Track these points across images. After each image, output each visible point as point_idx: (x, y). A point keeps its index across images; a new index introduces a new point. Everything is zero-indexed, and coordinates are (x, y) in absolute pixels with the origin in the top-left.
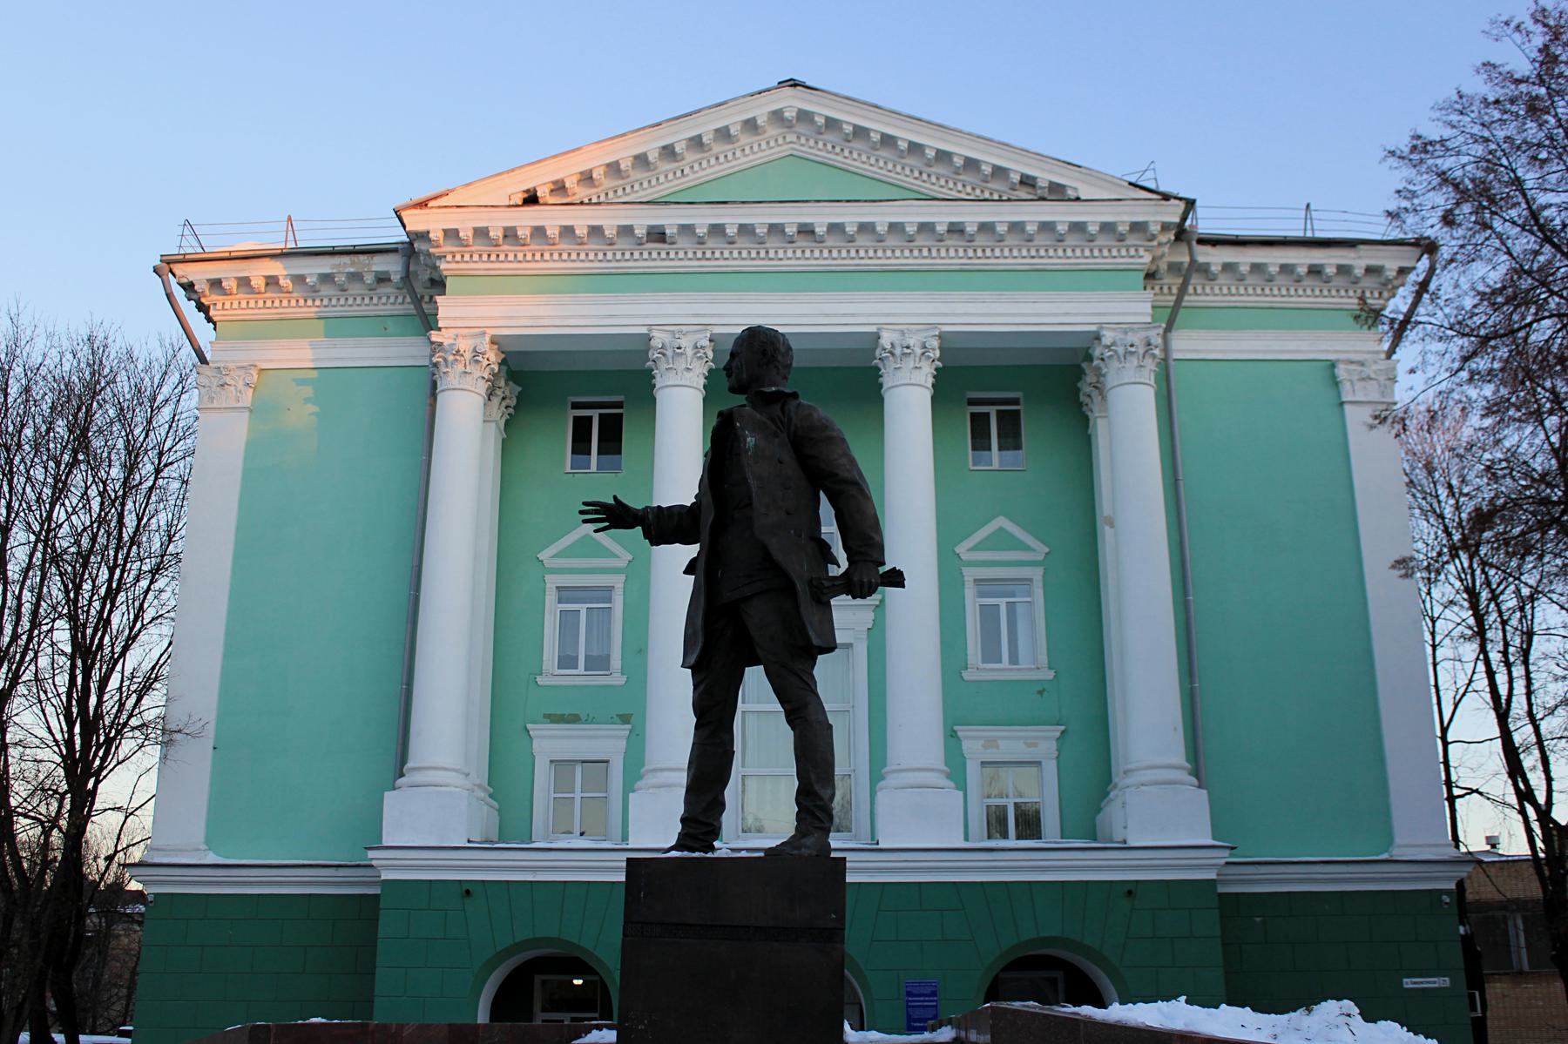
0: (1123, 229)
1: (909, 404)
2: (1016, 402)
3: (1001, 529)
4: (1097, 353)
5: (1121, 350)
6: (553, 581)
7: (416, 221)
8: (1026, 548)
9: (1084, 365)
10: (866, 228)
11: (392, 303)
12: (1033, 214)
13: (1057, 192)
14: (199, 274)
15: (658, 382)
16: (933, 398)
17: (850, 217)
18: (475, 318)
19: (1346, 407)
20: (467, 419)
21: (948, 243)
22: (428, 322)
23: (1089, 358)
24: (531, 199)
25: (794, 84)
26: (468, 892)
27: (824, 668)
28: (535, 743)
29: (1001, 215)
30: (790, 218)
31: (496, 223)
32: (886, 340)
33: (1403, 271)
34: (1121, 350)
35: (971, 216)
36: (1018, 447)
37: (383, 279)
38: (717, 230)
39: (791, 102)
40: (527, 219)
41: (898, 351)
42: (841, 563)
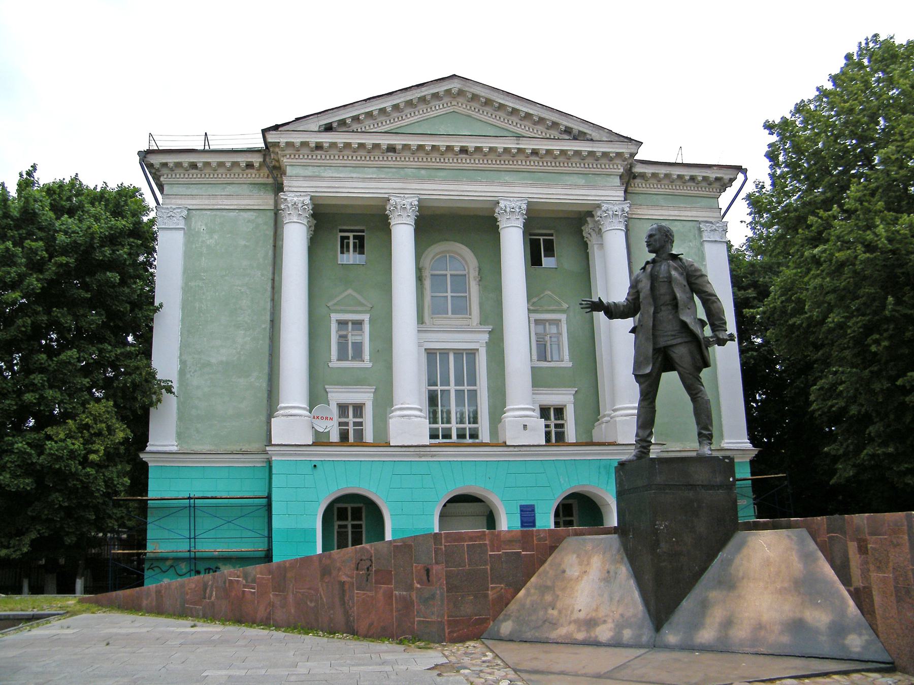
0: (599, 154)
1: (403, 236)
2: (363, 231)
3: (350, 294)
4: (497, 211)
5: (611, 213)
6: (335, 317)
7: (272, 137)
8: (365, 306)
9: (588, 219)
10: (361, 146)
11: (263, 177)
12: (572, 146)
13: (580, 136)
14: (156, 160)
15: (393, 222)
16: (415, 230)
17: (486, 144)
18: (302, 188)
19: (706, 245)
20: (296, 237)
21: (531, 158)
22: (279, 188)
23: (592, 216)
24: (329, 128)
25: (454, 76)
26: (315, 466)
27: (705, 374)
28: (329, 395)
29: (556, 146)
30: (457, 144)
31: (313, 139)
32: (502, 204)
33: (732, 180)
34: (611, 213)
35: (543, 146)
36: (363, 253)
37: (250, 165)
38: (421, 147)
39: (455, 86)
40: (326, 138)
41: (508, 210)
42: (708, 332)
